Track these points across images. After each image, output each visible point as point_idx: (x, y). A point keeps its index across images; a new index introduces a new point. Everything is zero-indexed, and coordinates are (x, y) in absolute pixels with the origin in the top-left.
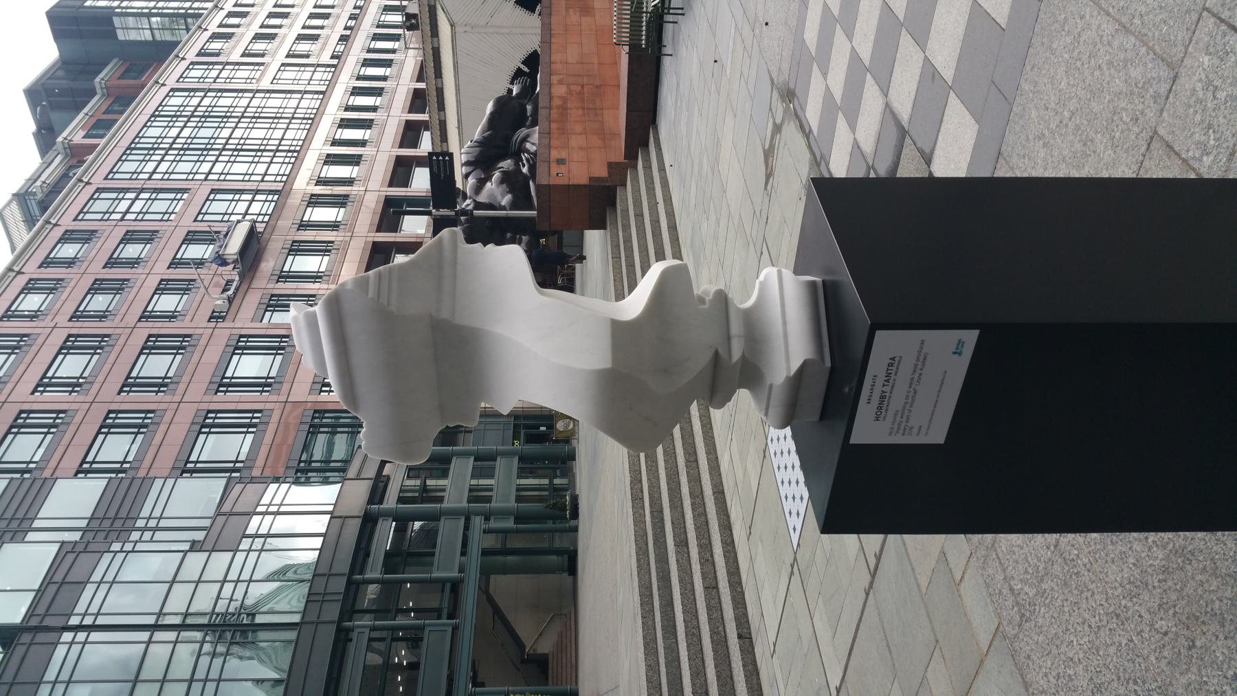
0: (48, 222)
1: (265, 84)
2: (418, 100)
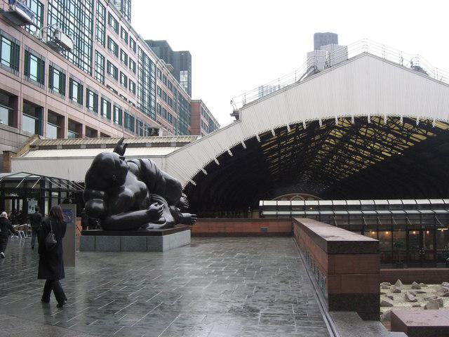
0: (122, 17)
1: (95, 47)
2: (76, 126)
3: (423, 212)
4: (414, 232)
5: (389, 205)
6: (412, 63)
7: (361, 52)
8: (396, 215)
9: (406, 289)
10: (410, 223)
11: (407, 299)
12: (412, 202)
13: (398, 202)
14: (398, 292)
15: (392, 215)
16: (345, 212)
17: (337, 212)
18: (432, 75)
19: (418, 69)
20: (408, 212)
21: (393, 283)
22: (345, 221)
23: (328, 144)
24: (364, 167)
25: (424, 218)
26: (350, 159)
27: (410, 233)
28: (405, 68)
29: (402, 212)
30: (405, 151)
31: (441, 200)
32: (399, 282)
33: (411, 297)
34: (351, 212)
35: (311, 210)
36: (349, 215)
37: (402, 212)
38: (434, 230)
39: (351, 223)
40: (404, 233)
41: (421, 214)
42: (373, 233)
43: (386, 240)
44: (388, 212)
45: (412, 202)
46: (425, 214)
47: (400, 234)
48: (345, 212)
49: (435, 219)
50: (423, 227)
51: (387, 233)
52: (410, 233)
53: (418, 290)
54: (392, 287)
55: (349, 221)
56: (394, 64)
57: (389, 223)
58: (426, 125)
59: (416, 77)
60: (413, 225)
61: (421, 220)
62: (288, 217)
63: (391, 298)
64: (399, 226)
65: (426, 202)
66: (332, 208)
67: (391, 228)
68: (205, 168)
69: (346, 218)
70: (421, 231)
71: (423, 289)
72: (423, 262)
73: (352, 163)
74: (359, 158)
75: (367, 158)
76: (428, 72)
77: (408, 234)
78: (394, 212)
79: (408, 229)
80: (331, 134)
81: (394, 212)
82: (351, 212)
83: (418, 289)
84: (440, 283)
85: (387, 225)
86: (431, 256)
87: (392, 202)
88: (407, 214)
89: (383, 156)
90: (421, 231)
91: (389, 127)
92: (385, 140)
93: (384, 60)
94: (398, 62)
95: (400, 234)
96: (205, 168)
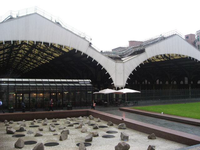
3: (58, 85)
4: (54, 94)
5: (42, 81)
6: (56, 21)
7: (33, 12)
8: (45, 86)
9: (49, 122)
10: (52, 89)
12: (71, 80)
13: (59, 80)
14: (46, 125)
15: (44, 86)
16: (21, 85)
17: (17, 84)
18: (63, 26)
19: (58, 23)
21: (43, 119)
22: (21, 88)
24: (31, 69)
25: (58, 87)
26: (26, 66)
27: (52, 94)
28: (53, 22)
29: (35, 85)
30: (50, 61)
32: (46, 119)
34: (24, 85)
35: (4, 83)
36: (23, 86)
37: (35, 85)
38: (62, 93)
40: (49, 94)
42: (35, 94)
43: (41, 97)
44: (42, 85)
46: (59, 86)
47: (47, 95)
48: (21, 85)
49: (63, 88)
50: (57, 92)
51: (41, 94)
52: (52, 94)
53: (56, 123)
54: (43, 121)
55: (23, 88)
56: (48, 19)
58: (59, 49)
59: (57, 26)
60: (53, 91)
61: (57, 88)
64: (46, 91)
65: (59, 80)
66: (15, 82)
67: (43, 92)
69: (22, 87)
70: (57, 93)
73: (27, 67)
75: (32, 65)
76: (62, 25)
77: (51, 95)
78: (44, 85)
79: (50, 92)
80: (19, 52)
81: (44, 85)
83: (55, 122)
85: (41, 91)
87: (56, 80)
89: (38, 65)
90: (57, 93)
91: (44, 50)
92: (37, 59)
93: (44, 17)
94: (50, 20)
95: (47, 95)
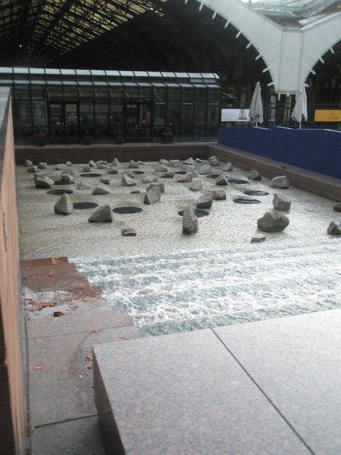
3: (141, 84)
11: (125, 184)
14: (115, 172)
16: (59, 83)
20: (111, 84)
21: (110, 160)
23: (45, 19)
24: (78, 44)
26: (66, 36)
31: (15, 72)
33: (128, 180)
39: (65, 95)
40: (122, 107)
41: (138, 87)
45: (129, 73)
47: (117, 108)
48: (59, 83)
49: (152, 93)
54: (108, 166)
55: (63, 92)
57: (106, 95)
60: (131, 99)
62: (26, 87)
63: (106, 183)
68: (252, 46)
71: (141, 169)
72: (139, 136)
74: (72, 35)
77: (125, 108)
82: (66, 83)
83: (135, 168)
84: (157, 160)
86: (148, 131)
88: (124, 87)
89: (94, 34)
96: (252, 46)
